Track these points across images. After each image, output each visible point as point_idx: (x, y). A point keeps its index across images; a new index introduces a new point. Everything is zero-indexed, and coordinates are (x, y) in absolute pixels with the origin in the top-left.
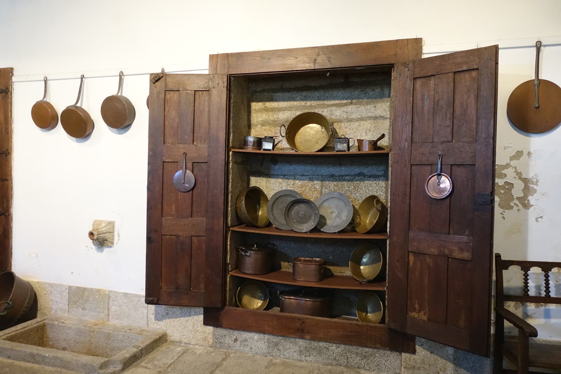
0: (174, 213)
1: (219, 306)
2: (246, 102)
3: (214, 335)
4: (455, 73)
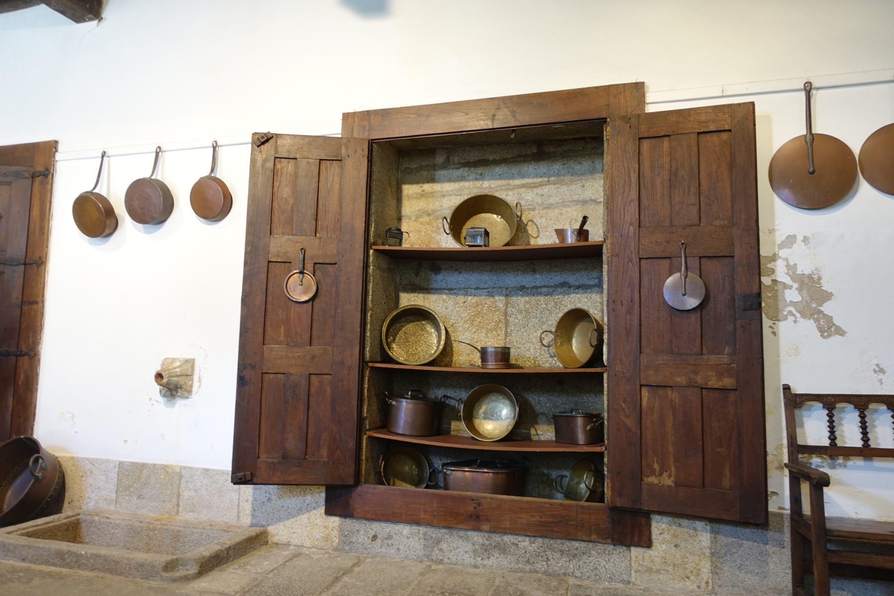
0: (282, 339)
1: (351, 482)
2: (394, 183)
3: (341, 530)
4: (699, 133)
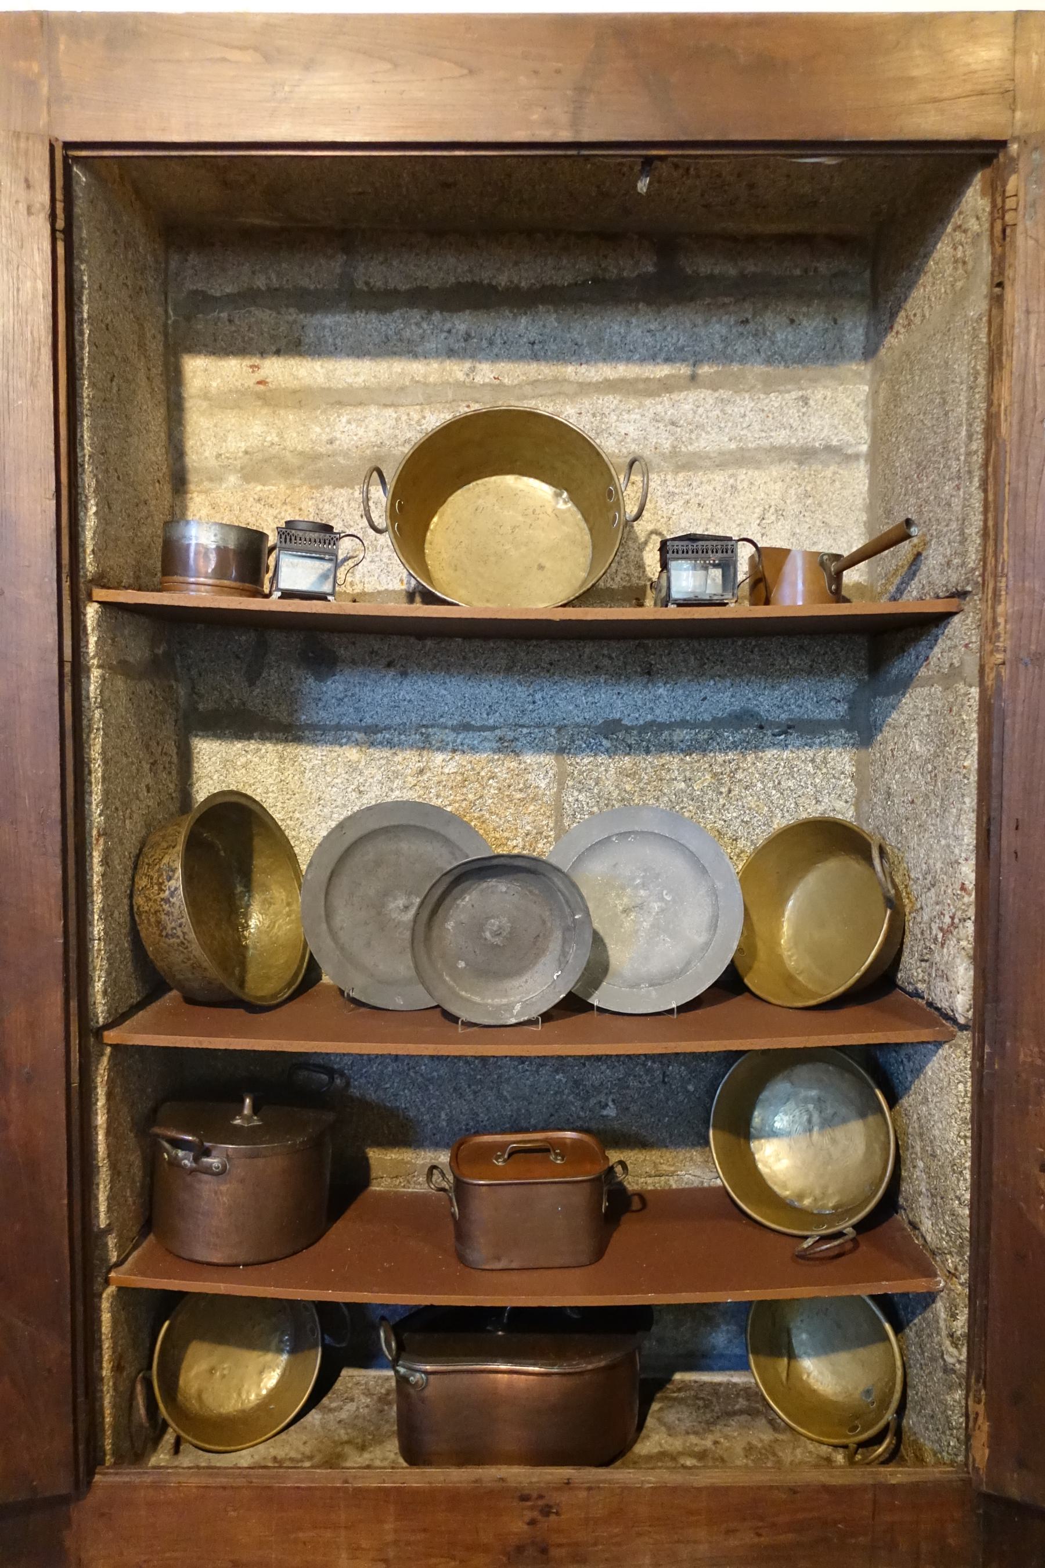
1: (63, 1485)
2: (155, 347)
